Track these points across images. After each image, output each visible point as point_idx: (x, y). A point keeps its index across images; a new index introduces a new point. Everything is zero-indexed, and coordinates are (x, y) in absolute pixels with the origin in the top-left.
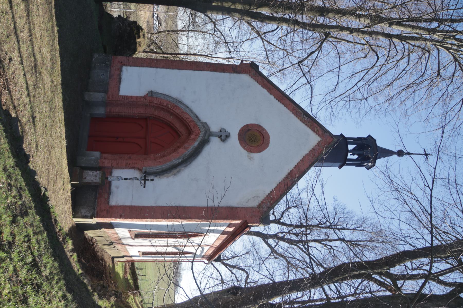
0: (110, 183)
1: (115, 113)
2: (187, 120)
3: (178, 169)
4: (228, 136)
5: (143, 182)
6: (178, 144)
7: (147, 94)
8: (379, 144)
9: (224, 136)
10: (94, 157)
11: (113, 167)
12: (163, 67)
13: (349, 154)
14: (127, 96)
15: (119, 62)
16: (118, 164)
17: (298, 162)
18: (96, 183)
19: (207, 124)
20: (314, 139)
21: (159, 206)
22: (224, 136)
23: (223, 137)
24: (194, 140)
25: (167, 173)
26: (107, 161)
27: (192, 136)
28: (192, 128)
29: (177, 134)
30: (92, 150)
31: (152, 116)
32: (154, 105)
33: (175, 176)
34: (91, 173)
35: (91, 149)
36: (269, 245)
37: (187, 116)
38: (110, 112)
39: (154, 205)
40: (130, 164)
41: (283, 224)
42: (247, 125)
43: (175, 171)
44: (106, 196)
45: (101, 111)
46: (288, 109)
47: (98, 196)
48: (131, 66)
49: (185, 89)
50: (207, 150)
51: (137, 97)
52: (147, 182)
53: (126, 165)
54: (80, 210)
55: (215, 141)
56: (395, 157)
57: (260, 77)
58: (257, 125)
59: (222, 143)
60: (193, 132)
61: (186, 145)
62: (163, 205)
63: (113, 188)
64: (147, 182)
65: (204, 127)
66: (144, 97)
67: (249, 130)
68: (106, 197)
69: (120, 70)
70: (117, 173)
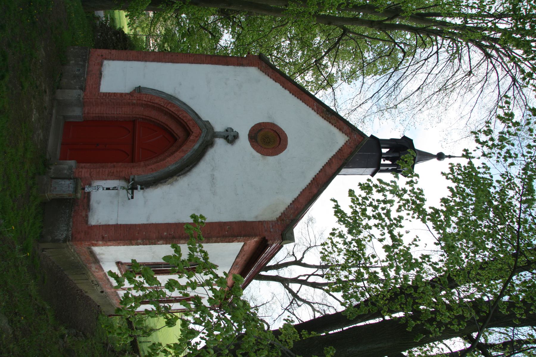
1: (94, 115)
2: (184, 119)
4: (236, 137)
7: (135, 90)
8: (417, 146)
9: (231, 137)
12: (153, 61)
13: (382, 160)
14: (109, 93)
15: (99, 56)
17: (323, 165)
19: (209, 123)
20: (341, 139)
22: (231, 137)
23: (230, 138)
24: (194, 142)
25: (161, 183)
26: (84, 170)
27: (192, 138)
28: (191, 128)
29: (174, 138)
30: (66, 160)
31: (141, 116)
32: (144, 102)
36: (291, 291)
37: (185, 114)
38: (88, 113)
39: (145, 222)
40: (113, 173)
41: (305, 265)
42: (259, 125)
45: (76, 113)
46: (307, 105)
48: (113, 60)
49: (181, 84)
50: (211, 154)
51: (121, 94)
55: (220, 142)
56: (435, 160)
57: (271, 70)
58: (271, 123)
59: (229, 146)
60: (193, 132)
61: (184, 148)
64: (135, 191)
65: (205, 125)
66: (131, 94)
67: (261, 130)
69: (101, 65)
70: (96, 183)
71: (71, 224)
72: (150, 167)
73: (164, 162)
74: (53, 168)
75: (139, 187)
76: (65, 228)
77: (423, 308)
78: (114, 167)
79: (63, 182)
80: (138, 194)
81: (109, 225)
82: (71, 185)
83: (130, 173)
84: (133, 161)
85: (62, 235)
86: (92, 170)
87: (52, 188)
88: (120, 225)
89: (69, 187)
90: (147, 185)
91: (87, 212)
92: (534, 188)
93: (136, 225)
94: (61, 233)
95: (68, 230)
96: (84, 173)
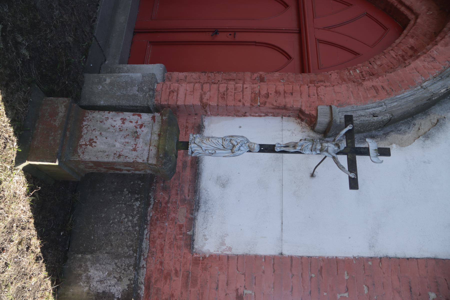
0: (196, 163)
3: (433, 117)
5: (343, 160)
6: (411, 41)
10: (139, 75)
11: (205, 109)
16: (224, 96)
18: (134, 164)
21: (389, 258)
26: (183, 88)
33: (428, 142)
34: (114, 120)
35: (136, 57)
39: (365, 253)
43: (424, 123)
44: (181, 216)
47: (151, 213)
52: (360, 160)
53: (254, 100)
54: (86, 270)
62: (400, 254)
63: (208, 184)
64: (360, 160)
68: (182, 220)
70: (218, 128)
72: (368, 84)
77: (24, 55)
78: (262, 80)
81: (256, 257)
88: (291, 258)
92: (2, 104)
96: (186, 90)
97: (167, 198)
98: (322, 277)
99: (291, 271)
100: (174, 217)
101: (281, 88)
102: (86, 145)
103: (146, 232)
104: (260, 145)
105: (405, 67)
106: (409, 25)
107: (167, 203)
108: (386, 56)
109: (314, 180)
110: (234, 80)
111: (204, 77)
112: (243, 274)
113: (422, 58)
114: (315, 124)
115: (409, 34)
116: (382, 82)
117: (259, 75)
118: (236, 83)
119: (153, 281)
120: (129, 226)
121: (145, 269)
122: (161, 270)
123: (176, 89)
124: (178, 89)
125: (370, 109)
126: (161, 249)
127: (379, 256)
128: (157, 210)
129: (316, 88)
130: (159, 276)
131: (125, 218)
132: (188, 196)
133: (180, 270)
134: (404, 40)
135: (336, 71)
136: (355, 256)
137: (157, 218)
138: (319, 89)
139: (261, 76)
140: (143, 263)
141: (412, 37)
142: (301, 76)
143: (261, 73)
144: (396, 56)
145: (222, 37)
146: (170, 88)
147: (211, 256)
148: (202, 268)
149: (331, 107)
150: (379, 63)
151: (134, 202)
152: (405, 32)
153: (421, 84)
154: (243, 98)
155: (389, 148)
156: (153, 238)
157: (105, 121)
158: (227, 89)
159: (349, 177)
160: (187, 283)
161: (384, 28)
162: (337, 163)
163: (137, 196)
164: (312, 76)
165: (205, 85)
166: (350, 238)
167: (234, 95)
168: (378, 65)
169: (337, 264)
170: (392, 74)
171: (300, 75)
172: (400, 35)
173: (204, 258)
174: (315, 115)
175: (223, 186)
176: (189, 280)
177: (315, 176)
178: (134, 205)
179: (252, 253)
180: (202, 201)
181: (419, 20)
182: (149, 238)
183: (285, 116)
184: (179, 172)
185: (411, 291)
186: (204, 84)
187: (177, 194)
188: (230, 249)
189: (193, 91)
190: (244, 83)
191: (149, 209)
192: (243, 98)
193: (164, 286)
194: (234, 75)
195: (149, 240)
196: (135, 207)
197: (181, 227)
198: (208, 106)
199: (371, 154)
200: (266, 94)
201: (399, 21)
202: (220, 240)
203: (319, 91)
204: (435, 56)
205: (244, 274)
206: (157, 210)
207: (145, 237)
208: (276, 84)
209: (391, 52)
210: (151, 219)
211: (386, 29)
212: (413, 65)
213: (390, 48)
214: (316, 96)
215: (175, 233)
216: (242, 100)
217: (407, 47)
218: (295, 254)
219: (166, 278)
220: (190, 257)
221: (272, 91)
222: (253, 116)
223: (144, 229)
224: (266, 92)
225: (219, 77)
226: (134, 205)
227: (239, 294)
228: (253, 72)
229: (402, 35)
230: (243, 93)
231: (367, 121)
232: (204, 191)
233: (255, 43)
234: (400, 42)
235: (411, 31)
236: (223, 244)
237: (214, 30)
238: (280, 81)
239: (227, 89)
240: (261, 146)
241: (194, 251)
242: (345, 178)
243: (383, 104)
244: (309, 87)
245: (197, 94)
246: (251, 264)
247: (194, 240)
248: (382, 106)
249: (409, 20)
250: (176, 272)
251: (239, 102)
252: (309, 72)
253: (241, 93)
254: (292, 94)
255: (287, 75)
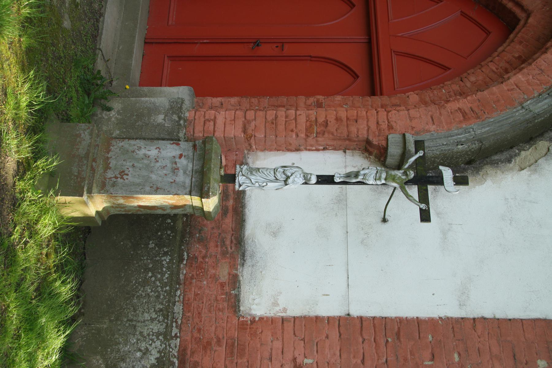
5: (414, 191)
20: (385, 145)
25: (495, 164)
39: (453, 311)
71: (178, 308)
72: (453, 106)
73: (504, 87)
74: (117, 105)
75: (447, 173)
76: (156, 327)
78: (319, 105)
79: (153, 152)
80: (447, 198)
81: (318, 319)
82: (184, 161)
83: (384, 126)
84: (373, 90)
85: (146, 352)
86: (250, 114)
87: (110, 174)
88: (361, 319)
89: (175, 170)
90: (469, 164)
91: (233, 266)
93: (418, 322)
94: (143, 345)
95: (167, 336)
96: (225, 119)
97: (204, 251)
98: (400, 341)
99: (361, 335)
100: (215, 275)
101: (343, 114)
102: (116, 177)
103: (178, 293)
104: (317, 176)
105: (502, 83)
106: (518, 27)
107: (204, 257)
108: (483, 70)
109: (386, 225)
110: (284, 106)
111: (245, 101)
112: (302, 340)
113: (525, 70)
114: (386, 158)
115: (516, 39)
116: (471, 103)
117: (315, 100)
118: (287, 110)
119: (189, 352)
120: (158, 286)
121: (178, 340)
122: (200, 339)
123: (213, 118)
124: (215, 117)
125: (453, 136)
126: (199, 313)
127: (472, 317)
128: (192, 266)
129: (386, 113)
130: (196, 346)
131: (151, 277)
132: (231, 249)
133: (223, 338)
134: (509, 47)
135: (416, 92)
136: (441, 316)
137: (193, 275)
138: (390, 114)
139: (318, 101)
140: (175, 331)
141: (520, 43)
142: (369, 100)
143: (319, 97)
144: (497, 69)
145: (266, 50)
146: (205, 117)
147: (261, 319)
148: (251, 334)
149: (404, 135)
150: (473, 79)
151: (162, 257)
152: (512, 36)
153: (521, 104)
154: (296, 127)
155: (467, 177)
156: (188, 300)
157: (137, 151)
158: (276, 117)
159: (420, 209)
160: (232, 353)
161: (486, 33)
162: (407, 196)
163: (165, 250)
164: (385, 99)
165: (248, 112)
166: (433, 294)
167: (285, 124)
168: (472, 82)
169: (419, 326)
170: (485, 92)
171: (368, 98)
172: (504, 42)
173: (253, 321)
174: (385, 146)
175: (275, 234)
176: (235, 349)
177: (388, 221)
178: (163, 261)
179: (312, 314)
180: (248, 254)
181: (531, 20)
182: (183, 301)
183: (349, 149)
184: (218, 220)
185: (515, 359)
186: (247, 110)
187: (217, 246)
188: (285, 310)
189: (234, 120)
190: (297, 110)
191: (182, 266)
192: (296, 127)
193: (202, 359)
194: (284, 99)
195: (183, 303)
196: (164, 263)
197: (222, 285)
198: (253, 137)
199: (445, 183)
200: (324, 121)
201: (508, 23)
202: (272, 300)
203: (390, 116)
204: (543, 68)
205: (303, 340)
206: (192, 266)
207: (177, 299)
208: (339, 109)
209: (490, 64)
210: (185, 277)
211: (488, 33)
212: (512, 81)
213: (490, 59)
214: (387, 122)
215: (215, 293)
216: (294, 129)
217: (513, 56)
218: (365, 315)
219: (205, 348)
220: (235, 321)
221: (331, 119)
222: (309, 150)
223: (176, 290)
224: (323, 119)
225: (265, 101)
226: (163, 261)
227: (298, 364)
228: (308, 95)
229: (508, 41)
230: (296, 121)
231: (449, 150)
232: (250, 241)
233: (309, 58)
234: (503, 51)
235: (519, 35)
236: (275, 304)
237: (254, 41)
238: (342, 107)
239: (276, 117)
240: (318, 176)
241: (241, 313)
242: (415, 210)
243: (471, 130)
244: (377, 112)
245: (240, 123)
246: (309, 328)
247: (239, 301)
248: (469, 132)
249: (519, 20)
250: (219, 341)
251: (291, 133)
252: (381, 94)
253: (294, 121)
254: (356, 122)
255: (351, 99)
